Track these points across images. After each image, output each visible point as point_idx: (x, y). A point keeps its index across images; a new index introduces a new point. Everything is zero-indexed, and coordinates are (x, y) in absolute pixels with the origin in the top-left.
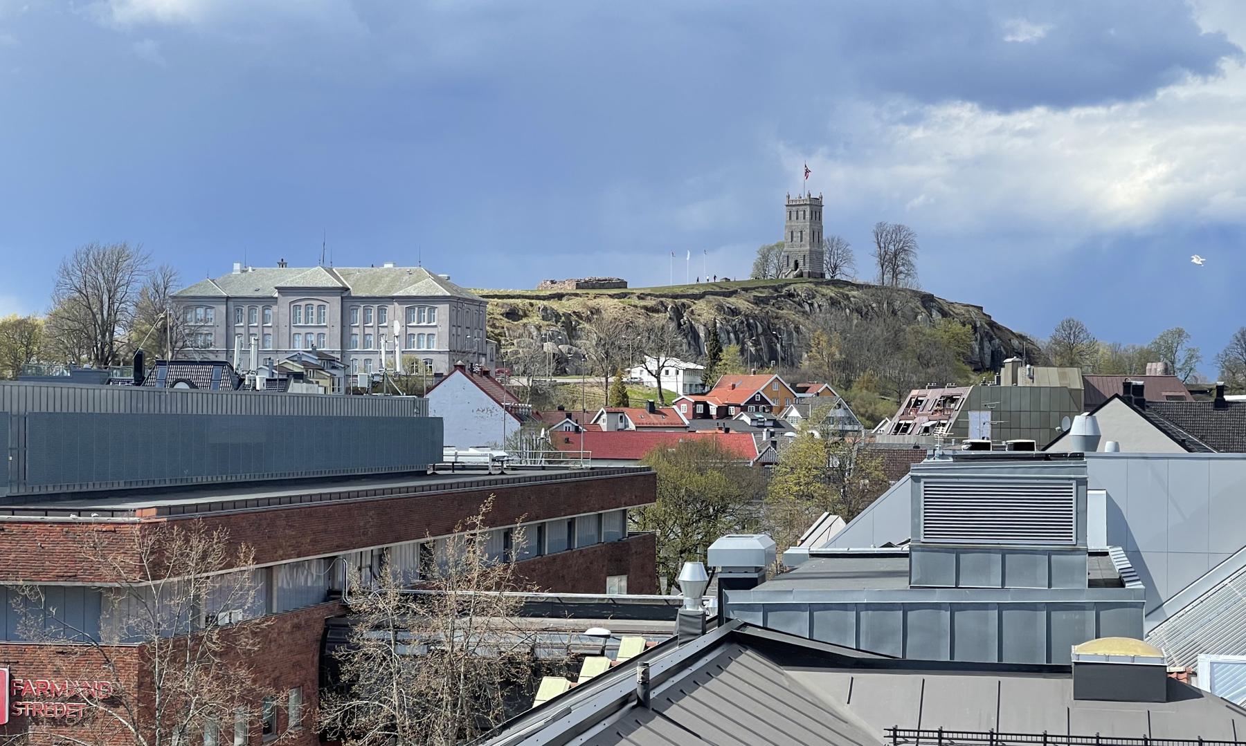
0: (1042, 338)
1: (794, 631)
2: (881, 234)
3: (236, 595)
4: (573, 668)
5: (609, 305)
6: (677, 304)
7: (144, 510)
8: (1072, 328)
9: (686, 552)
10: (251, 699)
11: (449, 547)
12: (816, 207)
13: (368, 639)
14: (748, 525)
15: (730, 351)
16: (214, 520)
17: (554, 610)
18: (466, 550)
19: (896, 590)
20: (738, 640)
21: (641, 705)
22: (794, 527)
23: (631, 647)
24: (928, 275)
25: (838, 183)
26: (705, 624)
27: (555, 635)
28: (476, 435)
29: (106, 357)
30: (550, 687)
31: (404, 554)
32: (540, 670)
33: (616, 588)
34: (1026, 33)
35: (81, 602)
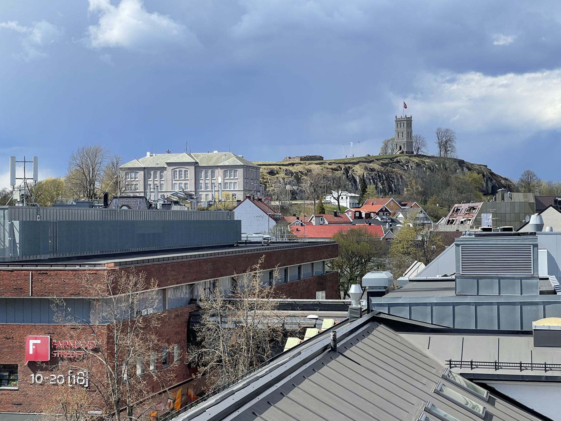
0: (515, 180)
1: (402, 316)
2: (439, 133)
3: (150, 301)
4: (301, 334)
5: (315, 168)
6: (347, 166)
7: (109, 264)
8: (529, 174)
9: (353, 280)
10: (157, 349)
11: (245, 279)
12: (409, 121)
13: (209, 321)
14: (381, 267)
15: (371, 188)
16: (140, 268)
17: (293, 307)
18: (252, 280)
19: (449, 296)
20: (377, 320)
21: (332, 350)
22: (402, 268)
23: (328, 323)
24: (461, 151)
25: (417, 110)
26: (361, 313)
27: (293, 318)
28: (256, 226)
29: (92, 195)
30: (291, 342)
31: (224, 282)
32: (286, 334)
33: (321, 297)
34: (503, 40)
35: (81, 306)
